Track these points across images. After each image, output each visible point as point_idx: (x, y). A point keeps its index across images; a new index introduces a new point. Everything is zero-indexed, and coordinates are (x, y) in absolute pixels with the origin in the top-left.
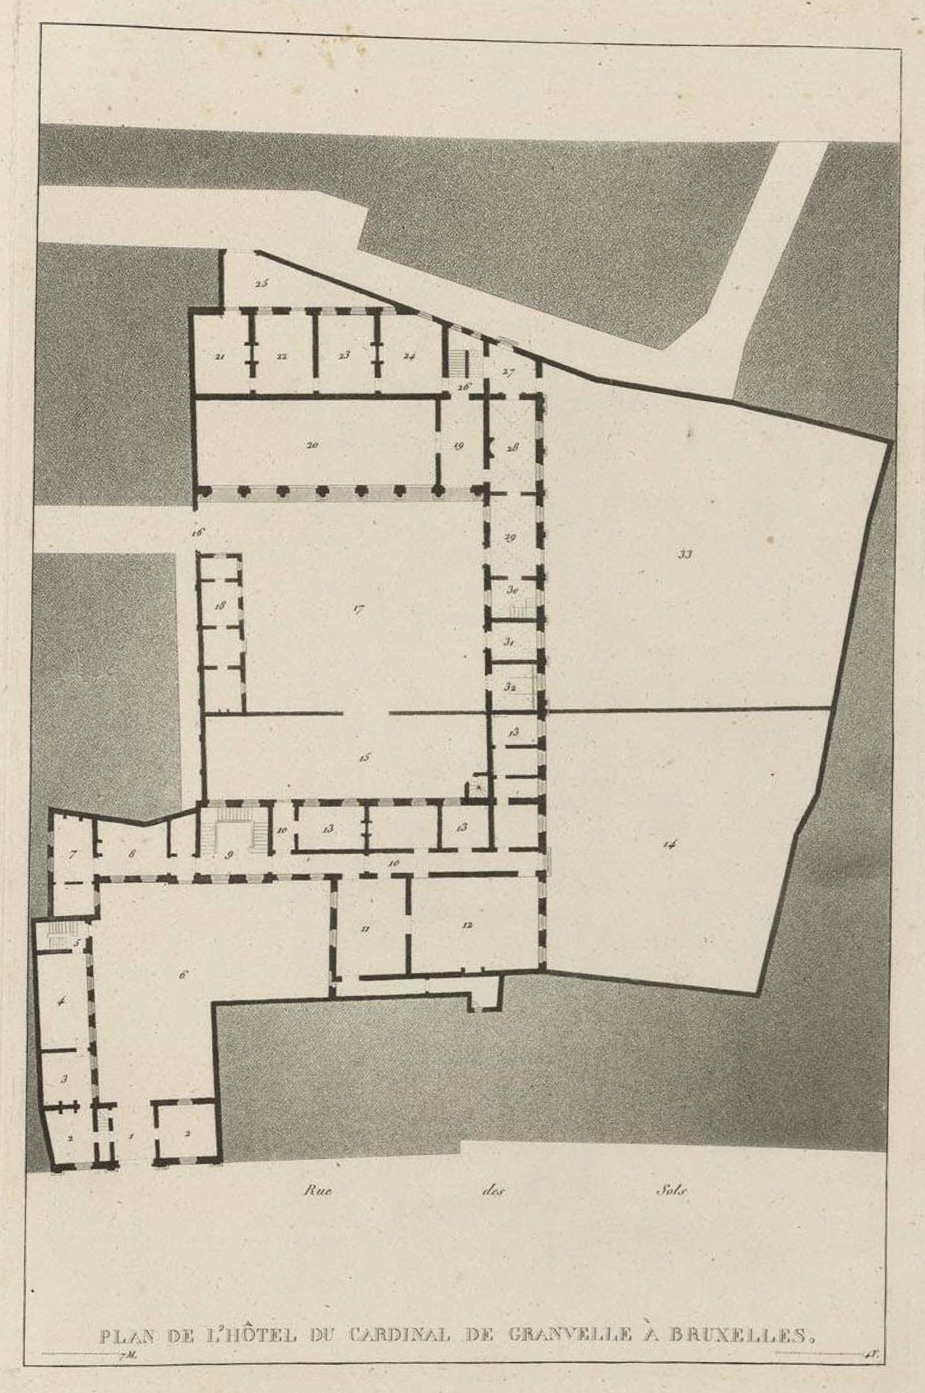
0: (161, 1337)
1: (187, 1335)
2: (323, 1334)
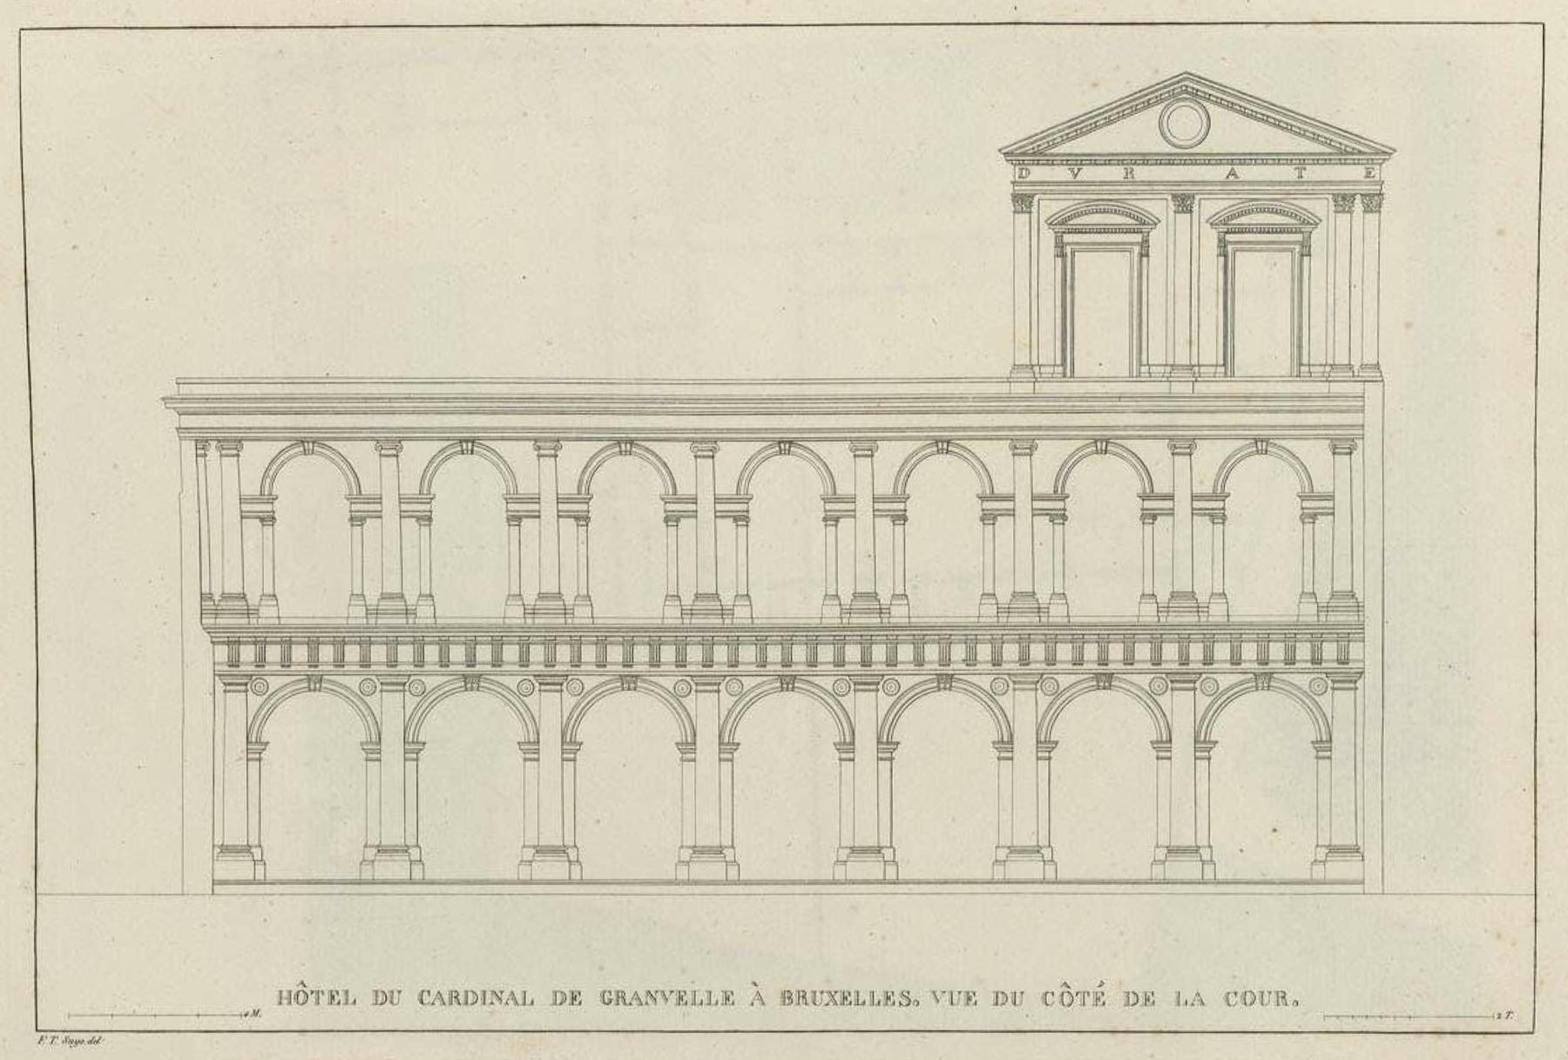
0: (984, 998)
1: (574, 998)
2: (385, 998)
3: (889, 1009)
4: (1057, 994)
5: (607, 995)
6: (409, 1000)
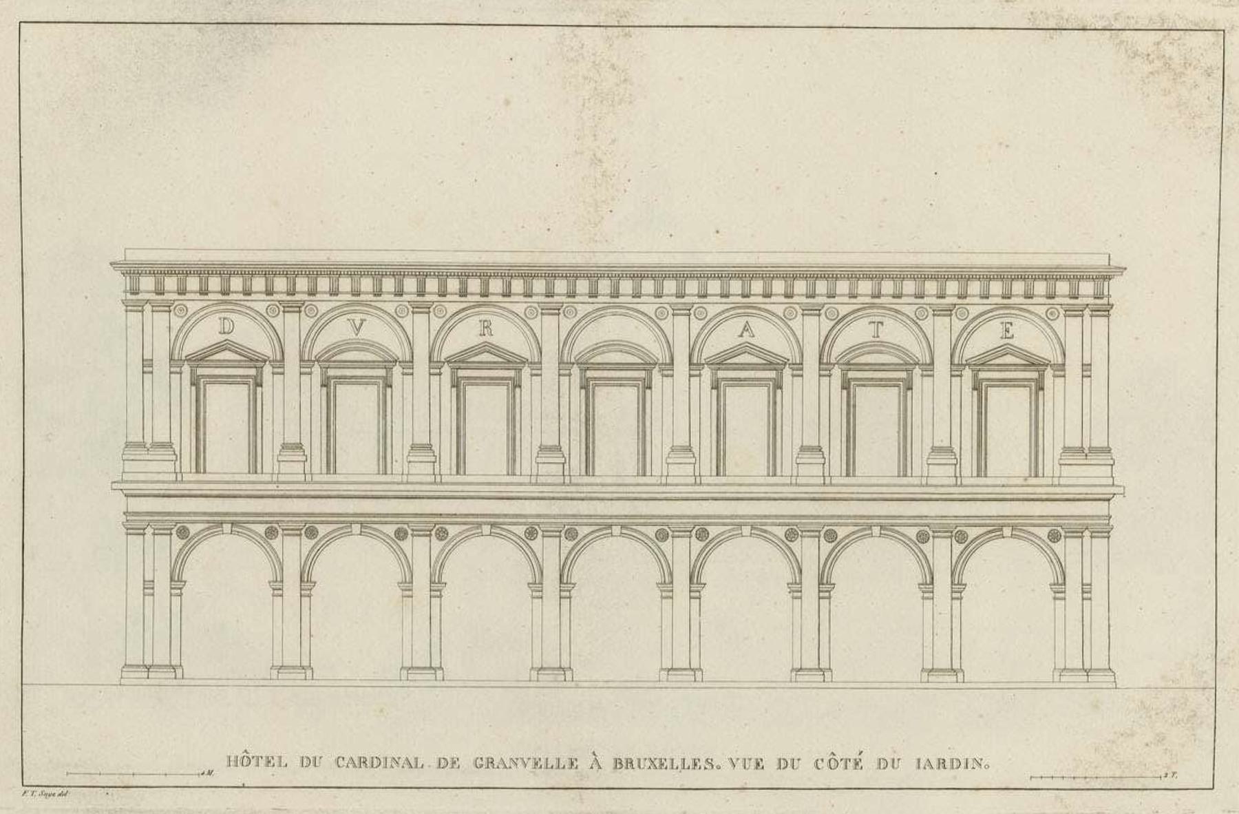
2: (310, 762)
3: (697, 771)
4: (826, 761)
5: (479, 762)
6: (806, 766)
